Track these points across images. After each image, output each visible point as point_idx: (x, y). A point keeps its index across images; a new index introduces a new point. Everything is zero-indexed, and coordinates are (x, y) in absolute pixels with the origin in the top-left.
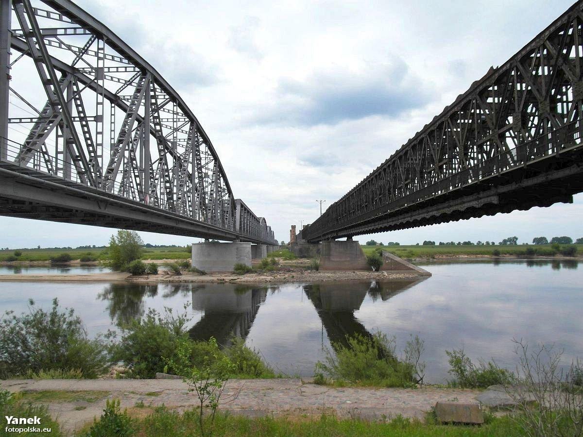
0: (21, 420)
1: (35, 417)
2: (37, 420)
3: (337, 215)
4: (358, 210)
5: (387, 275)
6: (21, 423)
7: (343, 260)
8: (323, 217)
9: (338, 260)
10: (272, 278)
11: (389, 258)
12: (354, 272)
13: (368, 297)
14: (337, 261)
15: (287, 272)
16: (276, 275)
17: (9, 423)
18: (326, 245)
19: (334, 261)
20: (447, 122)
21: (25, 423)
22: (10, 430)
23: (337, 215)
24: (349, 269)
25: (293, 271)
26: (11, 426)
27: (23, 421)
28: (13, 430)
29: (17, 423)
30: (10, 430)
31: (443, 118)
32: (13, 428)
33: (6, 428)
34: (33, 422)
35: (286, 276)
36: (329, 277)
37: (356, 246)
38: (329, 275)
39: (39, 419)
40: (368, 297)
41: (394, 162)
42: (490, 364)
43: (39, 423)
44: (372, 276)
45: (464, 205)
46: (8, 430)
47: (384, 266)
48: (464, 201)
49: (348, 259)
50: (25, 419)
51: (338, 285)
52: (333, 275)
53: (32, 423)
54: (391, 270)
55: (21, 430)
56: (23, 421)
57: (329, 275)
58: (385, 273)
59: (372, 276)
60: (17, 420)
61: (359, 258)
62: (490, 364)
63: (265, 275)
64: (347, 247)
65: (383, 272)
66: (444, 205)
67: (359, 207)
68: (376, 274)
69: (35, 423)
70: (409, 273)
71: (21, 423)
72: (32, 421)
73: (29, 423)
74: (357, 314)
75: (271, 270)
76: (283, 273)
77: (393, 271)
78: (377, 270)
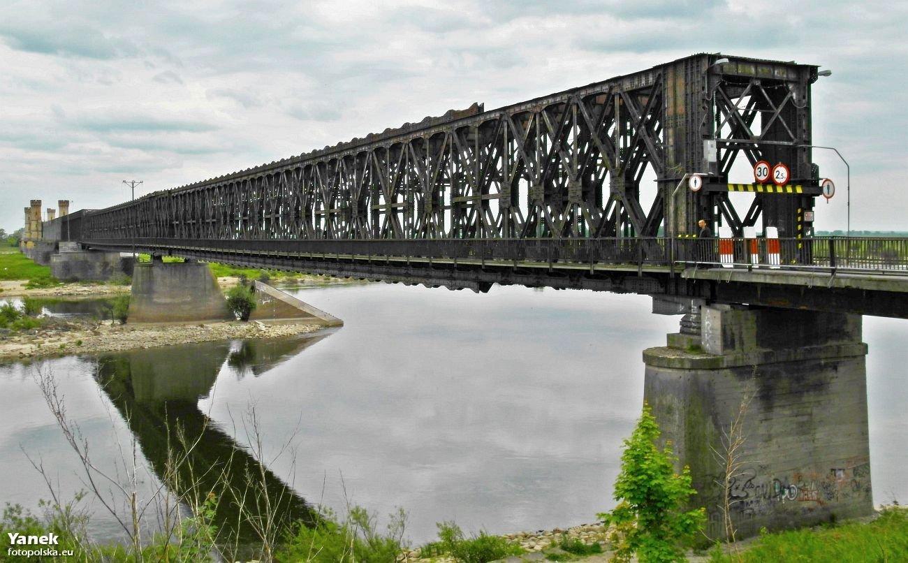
0: (30, 538)
1: (51, 534)
2: (53, 539)
3: (171, 215)
4: (225, 223)
5: (264, 328)
6: (30, 543)
7: (177, 301)
8: (132, 206)
9: (168, 300)
10: (33, 346)
11: (268, 295)
12: (202, 326)
13: (226, 372)
14: (165, 304)
15: (63, 330)
16: (41, 339)
17: (13, 543)
18: (143, 272)
19: (160, 304)
20: (407, 147)
21: (36, 543)
22: (15, 553)
23: (171, 215)
24: (189, 319)
25: (75, 329)
26: (15, 547)
27: (33, 540)
28: (18, 552)
29: (24, 543)
30: (15, 553)
31: (401, 139)
32: (19, 551)
33: (9, 551)
34: (48, 541)
35: (64, 340)
36: (154, 339)
37: (205, 272)
38: (154, 333)
39: (56, 537)
40: (226, 372)
41: (308, 168)
42: (481, 532)
43: (56, 543)
44: (235, 332)
45: (430, 280)
46: (11, 552)
47: (258, 310)
48: (430, 274)
49: (189, 299)
50: (35, 538)
51: (173, 353)
52: (161, 333)
53: (46, 543)
54: (271, 317)
55: (31, 553)
56: (33, 540)
57: (154, 333)
58: (262, 326)
59: (235, 332)
60: (24, 538)
61: (210, 296)
62: (481, 532)
63: (16, 342)
64: (186, 275)
65: (256, 323)
66: (399, 270)
67: (228, 218)
68: (244, 327)
69: (51, 543)
70: (304, 323)
71: (30, 543)
72: (47, 539)
73: (41, 542)
74: (203, 405)
75: (27, 328)
76: (55, 335)
77: (274, 320)
78: (245, 319)
